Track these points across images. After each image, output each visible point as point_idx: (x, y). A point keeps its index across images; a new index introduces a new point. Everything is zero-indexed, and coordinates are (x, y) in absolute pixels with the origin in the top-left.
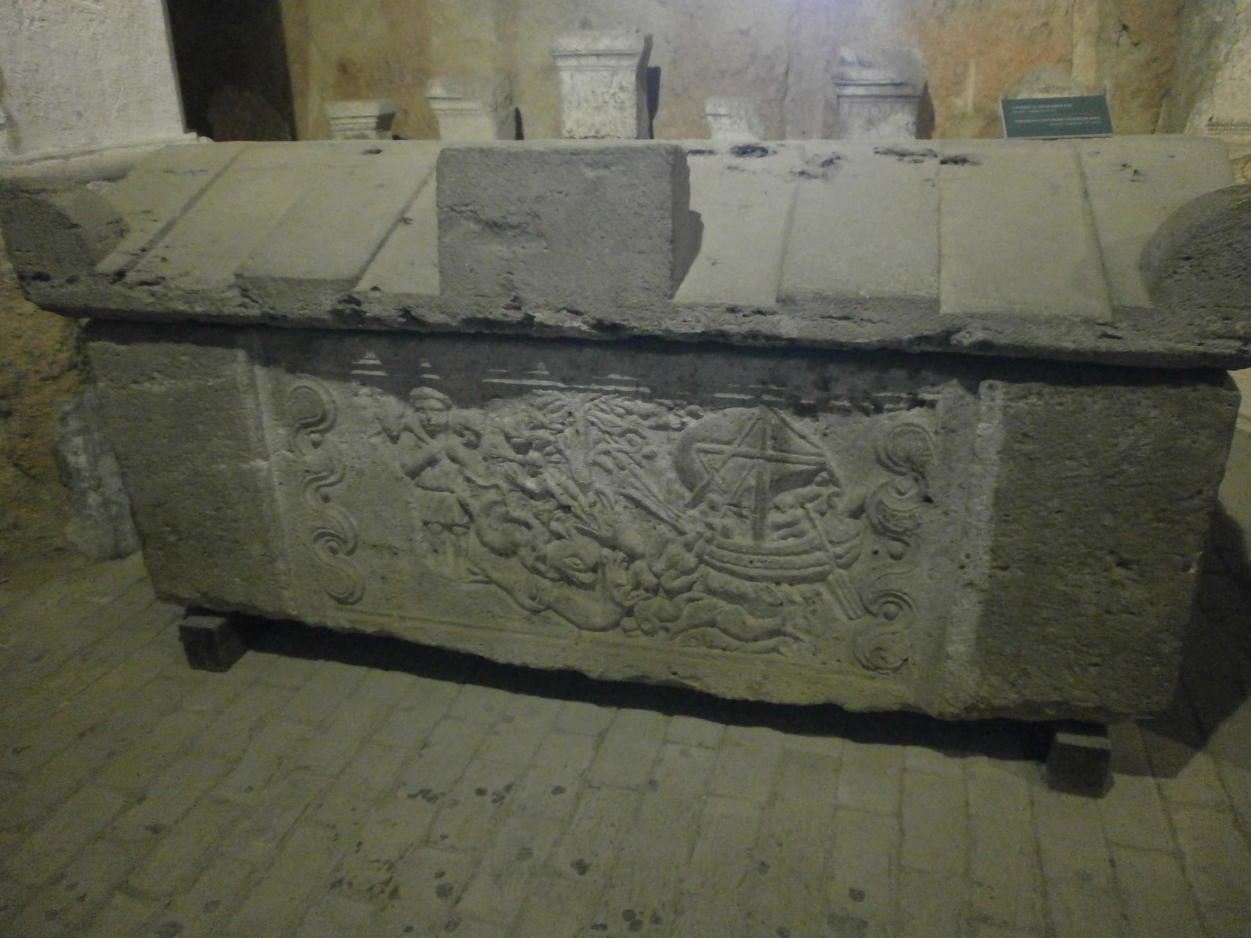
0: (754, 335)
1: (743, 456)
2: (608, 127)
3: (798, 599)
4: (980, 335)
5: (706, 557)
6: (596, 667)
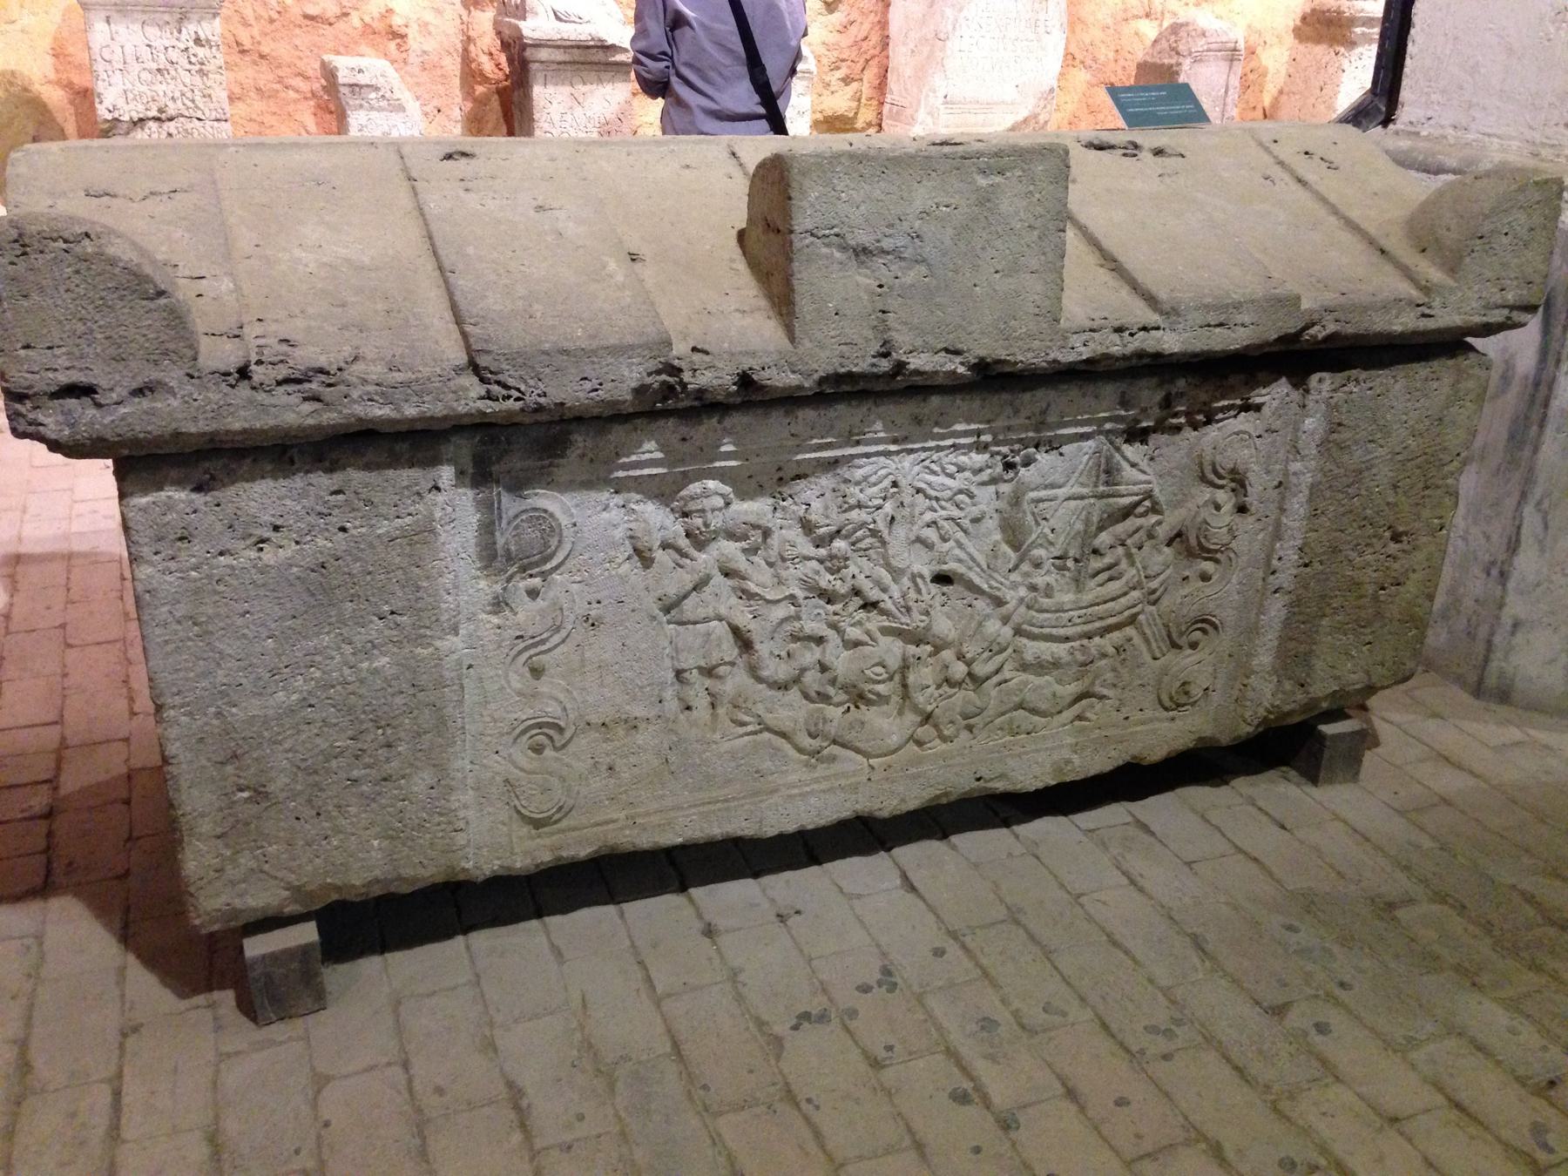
0: (1140, 354)
1: (1075, 499)
2: (179, 102)
3: (1111, 651)
4: (1332, 328)
5: (1025, 627)
6: (890, 800)
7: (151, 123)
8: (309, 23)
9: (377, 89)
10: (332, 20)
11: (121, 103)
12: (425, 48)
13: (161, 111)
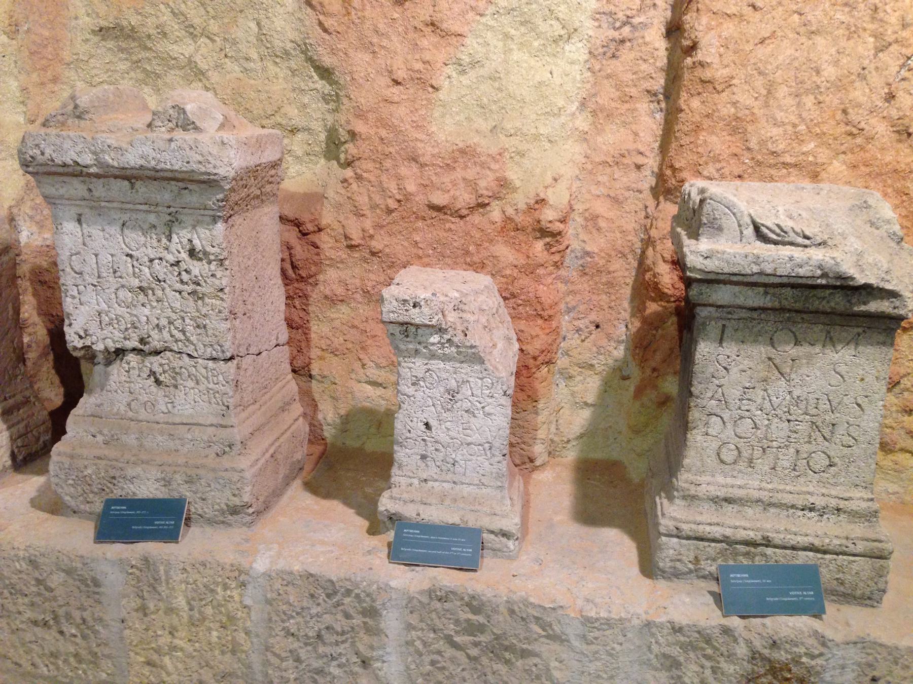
7: (131, 357)
8: (435, 214)
9: (441, 330)
10: (464, 212)
11: (93, 328)
12: (588, 249)
13: (142, 341)
